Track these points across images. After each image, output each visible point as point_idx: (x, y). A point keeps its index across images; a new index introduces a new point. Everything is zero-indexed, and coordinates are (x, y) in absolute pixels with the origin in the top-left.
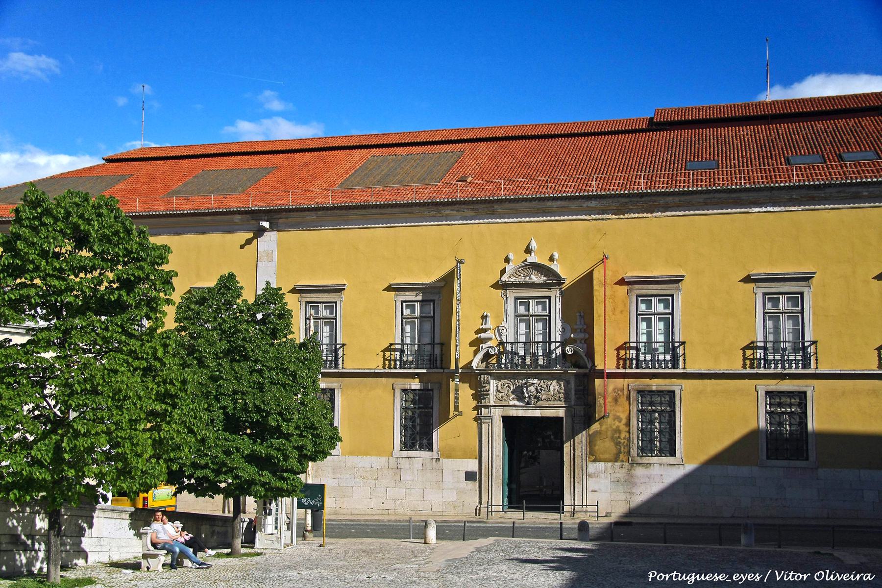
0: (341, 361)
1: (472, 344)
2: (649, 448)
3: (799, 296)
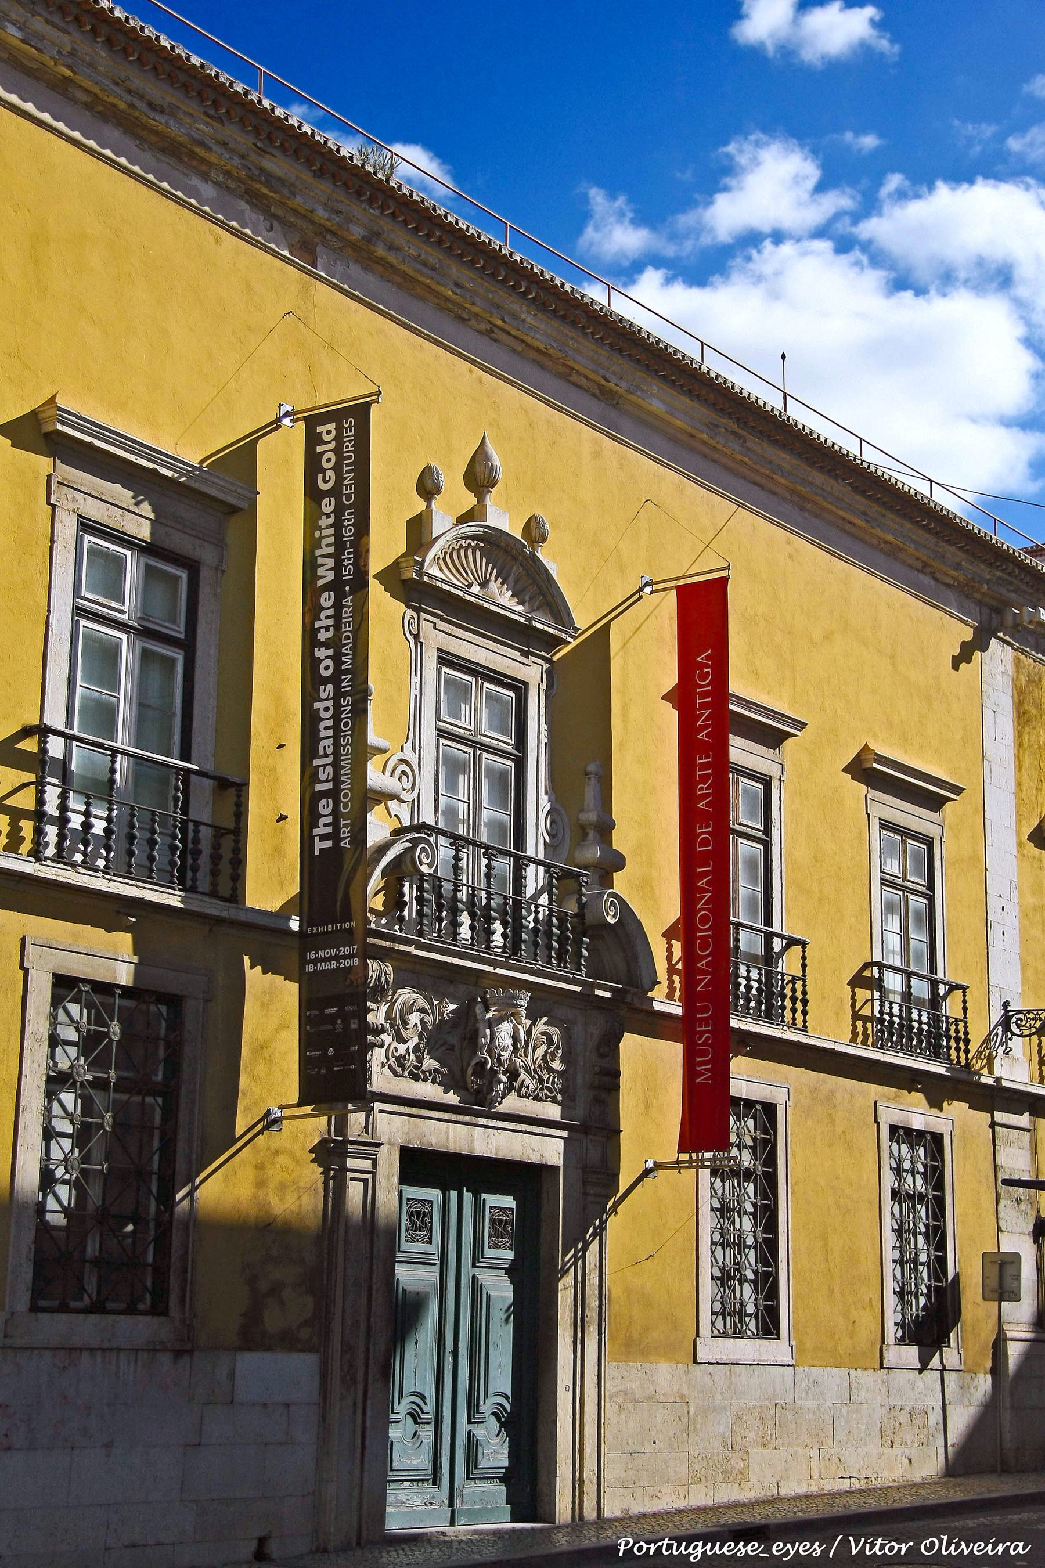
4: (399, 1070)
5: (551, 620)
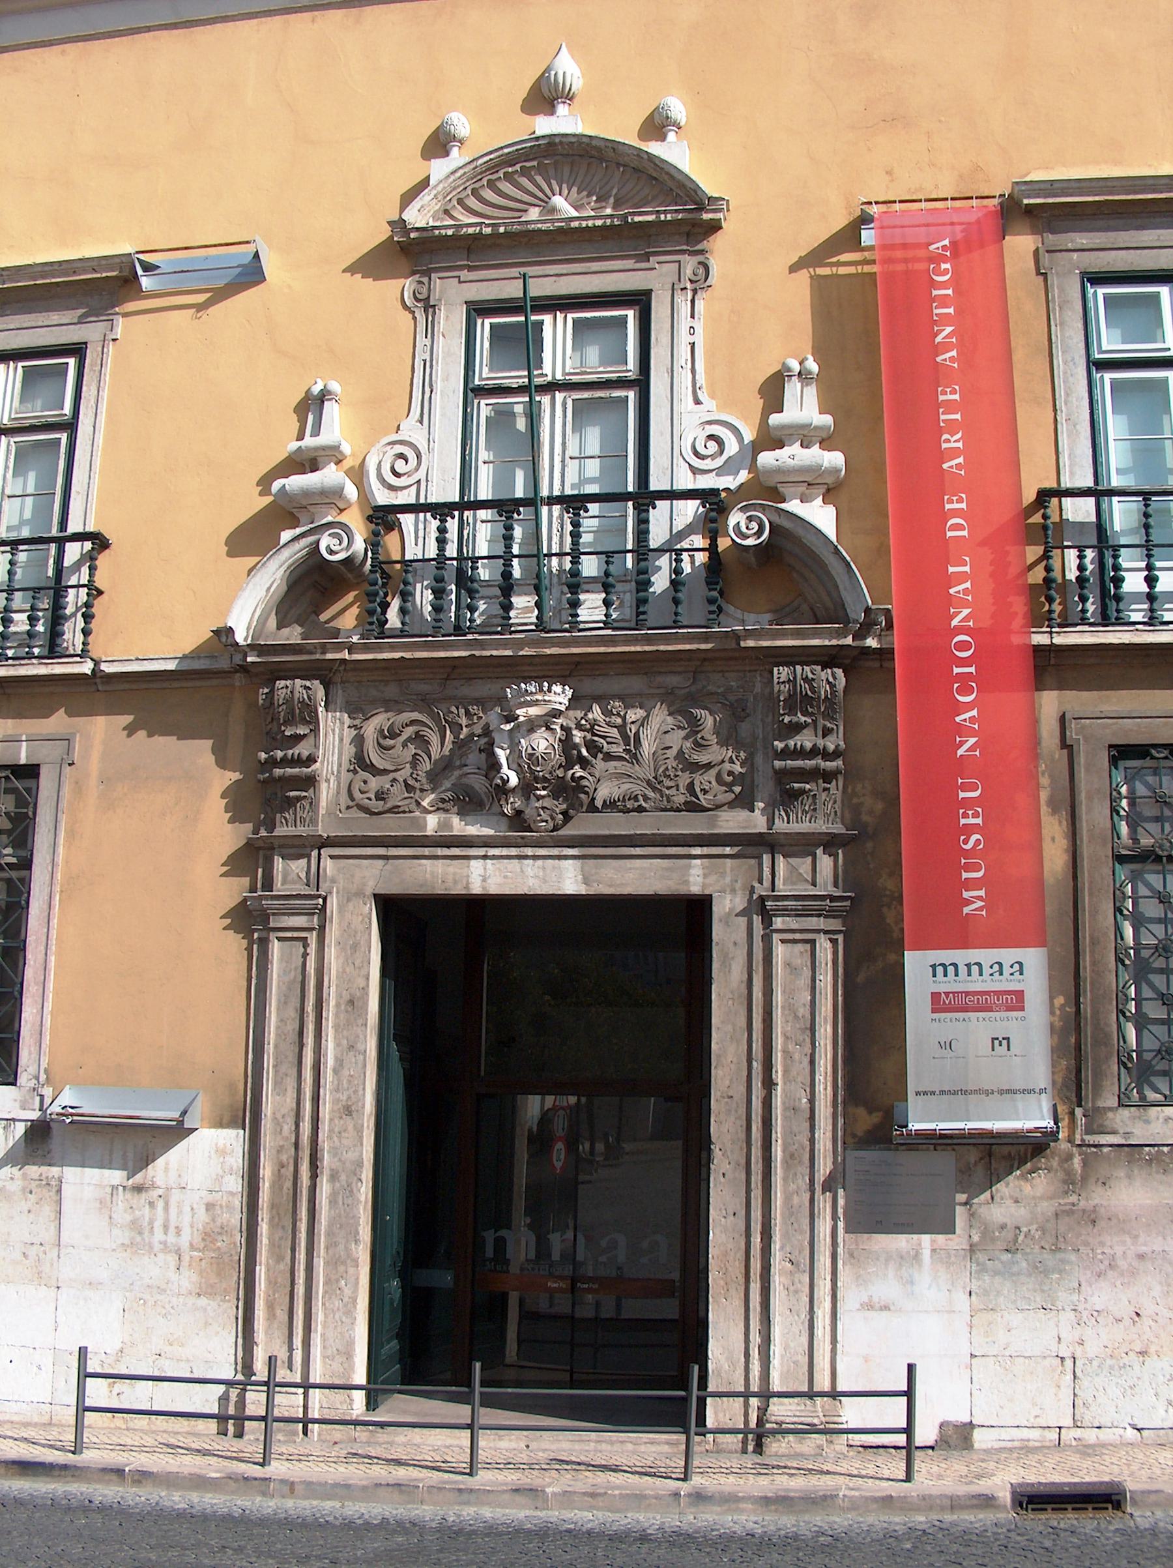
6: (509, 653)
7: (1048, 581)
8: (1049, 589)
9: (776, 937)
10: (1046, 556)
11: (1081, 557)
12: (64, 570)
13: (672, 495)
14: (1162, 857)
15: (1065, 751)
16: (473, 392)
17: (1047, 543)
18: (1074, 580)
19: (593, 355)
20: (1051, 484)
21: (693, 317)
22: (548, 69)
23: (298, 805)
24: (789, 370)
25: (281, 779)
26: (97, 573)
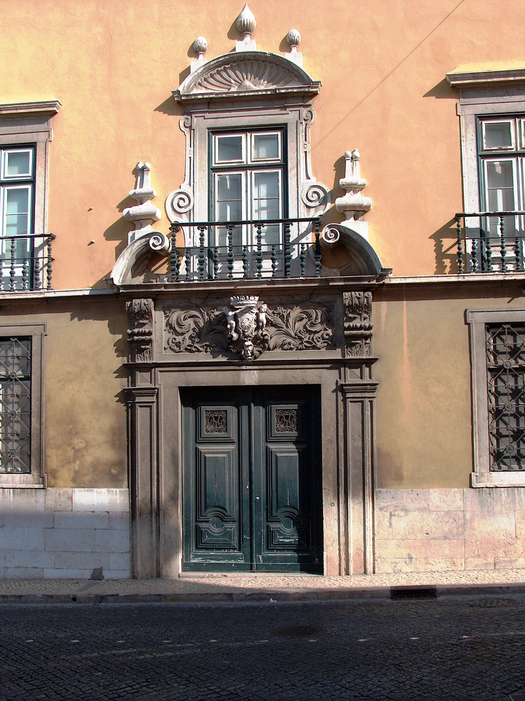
0: (46, 275)
1: (110, 234)
2: (515, 453)
3: (279, 133)
4: (177, 349)
5: (300, 84)
6: (233, 288)
7: (459, 254)
8: (460, 257)
9: (348, 400)
10: (458, 242)
11: (473, 243)
12: (35, 249)
13: (298, 220)
14: (507, 369)
15: (467, 326)
16: (213, 170)
17: (459, 237)
18: (470, 253)
19: (263, 152)
20: (461, 212)
21: (306, 140)
22: (239, 17)
23: (145, 351)
24: (348, 156)
25: (138, 341)
26: (52, 251)
